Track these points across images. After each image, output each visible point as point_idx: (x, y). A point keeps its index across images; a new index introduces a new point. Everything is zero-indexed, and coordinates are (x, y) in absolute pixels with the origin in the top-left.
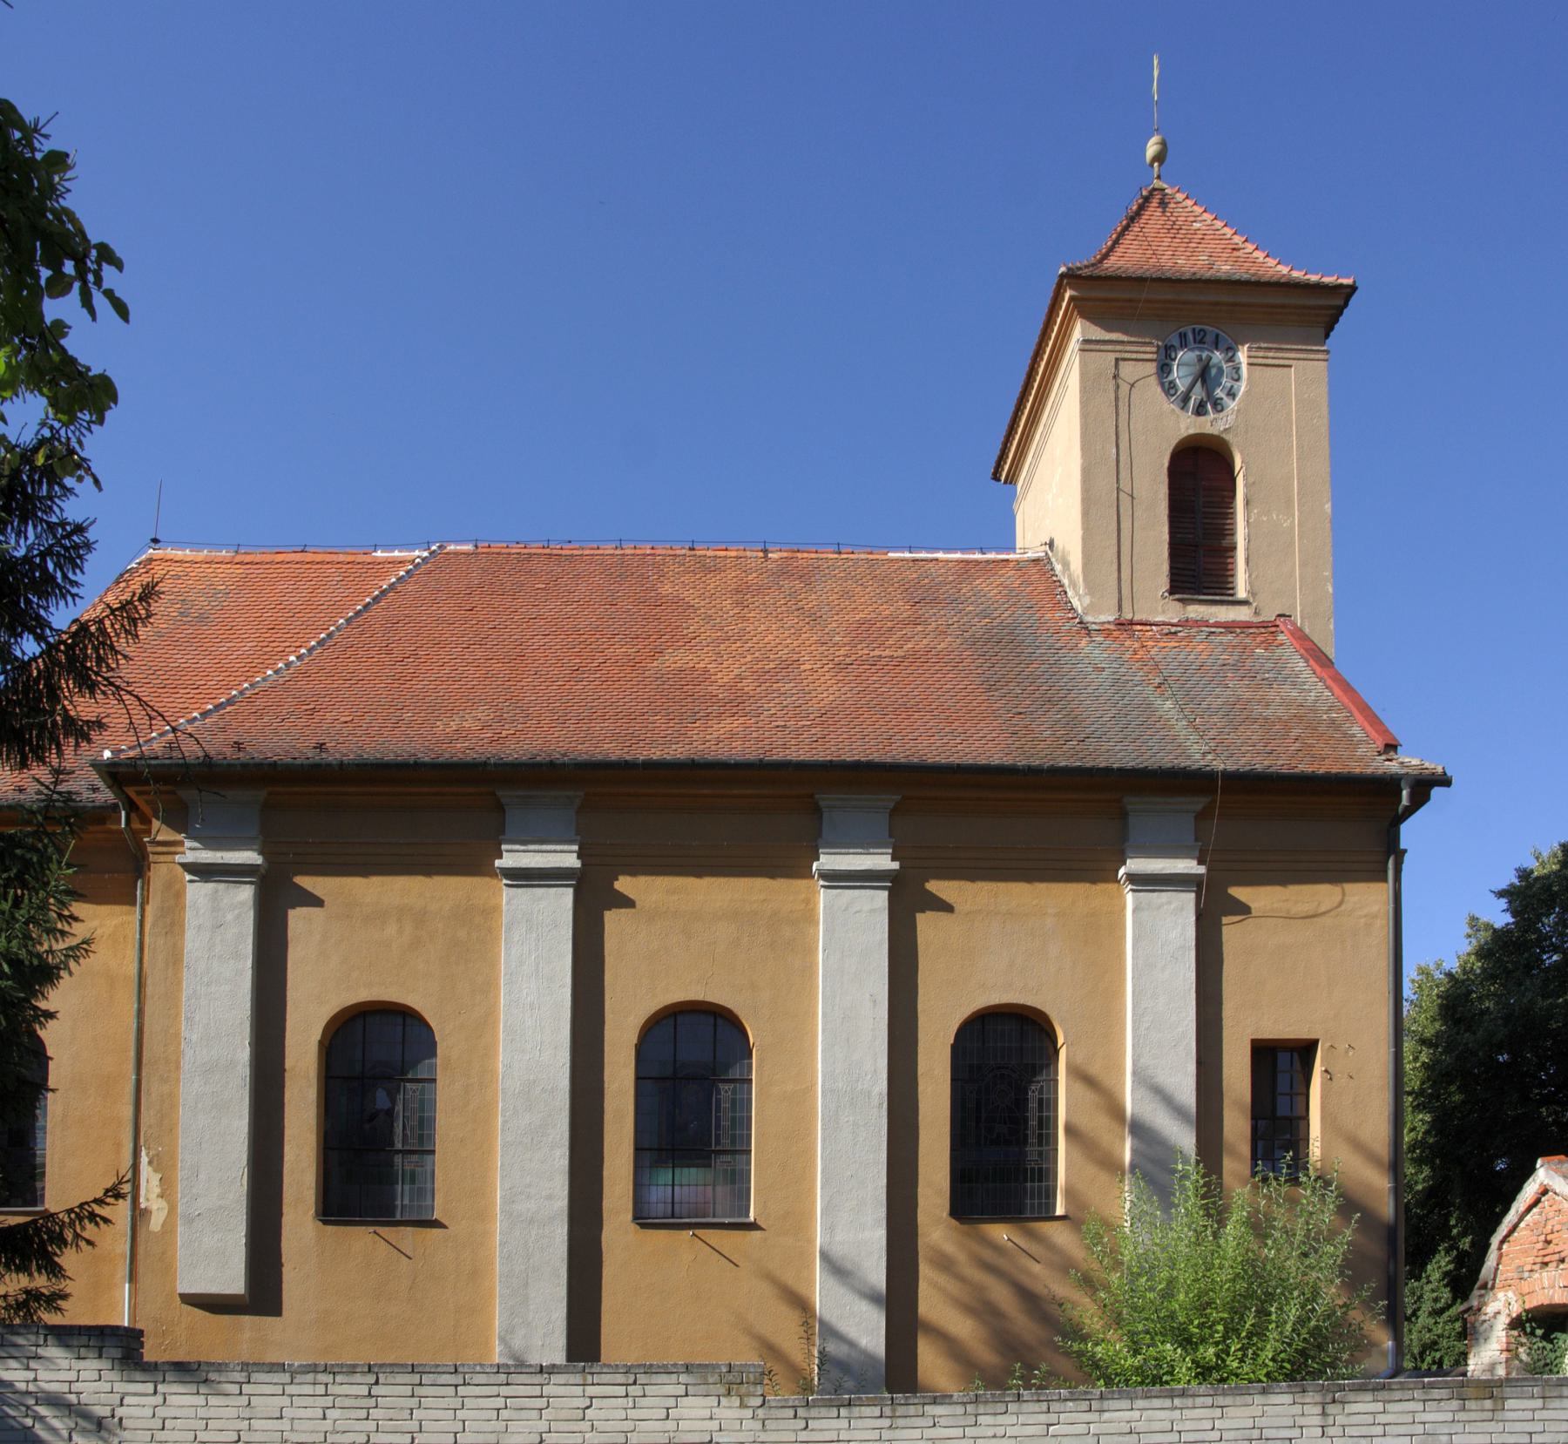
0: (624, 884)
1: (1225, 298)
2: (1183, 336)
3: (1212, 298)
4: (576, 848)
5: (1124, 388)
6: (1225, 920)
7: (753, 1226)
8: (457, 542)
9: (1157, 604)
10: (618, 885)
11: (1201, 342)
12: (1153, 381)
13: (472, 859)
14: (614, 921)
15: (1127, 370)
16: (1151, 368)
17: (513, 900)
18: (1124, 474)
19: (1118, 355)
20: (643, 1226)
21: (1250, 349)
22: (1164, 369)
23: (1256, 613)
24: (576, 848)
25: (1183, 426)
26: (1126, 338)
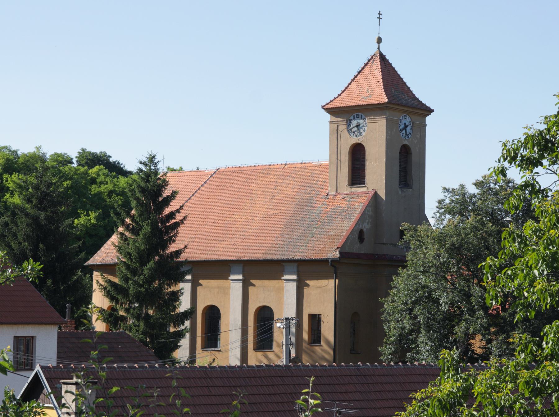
0: (253, 281)
2: (354, 116)
5: (339, 132)
9: (345, 189)
10: (251, 281)
12: (346, 130)
13: (225, 277)
15: (340, 127)
16: (345, 127)
22: (349, 125)
23: (368, 189)
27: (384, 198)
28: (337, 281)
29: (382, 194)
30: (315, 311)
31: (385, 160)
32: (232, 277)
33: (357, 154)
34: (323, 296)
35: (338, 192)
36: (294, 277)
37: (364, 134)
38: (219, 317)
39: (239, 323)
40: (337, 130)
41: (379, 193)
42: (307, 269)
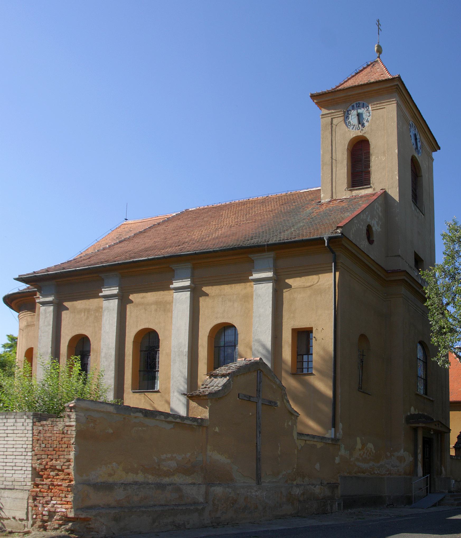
0: (205, 289)
1: (360, 91)
2: (353, 106)
3: (356, 92)
4: (118, 288)
5: (334, 126)
6: (284, 291)
7: (158, 392)
8: (191, 208)
11: (359, 107)
12: (343, 122)
14: (202, 300)
15: (335, 121)
16: (342, 119)
17: (106, 304)
18: (334, 154)
19: (332, 117)
20: (133, 392)
21: (371, 105)
23: (374, 189)
24: (118, 288)
25: (351, 135)
26: (333, 111)
27: (397, 198)
28: (337, 274)
29: (394, 193)
30: (302, 324)
31: (397, 151)
32: (176, 284)
33: (359, 153)
34: (315, 300)
35: (334, 198)
36: (270, 274)
37: (366, 124)
38: (158, 347)
39: (185, 349)
40: (332, 123)
41: (390, 193)
42: (288, 255)
